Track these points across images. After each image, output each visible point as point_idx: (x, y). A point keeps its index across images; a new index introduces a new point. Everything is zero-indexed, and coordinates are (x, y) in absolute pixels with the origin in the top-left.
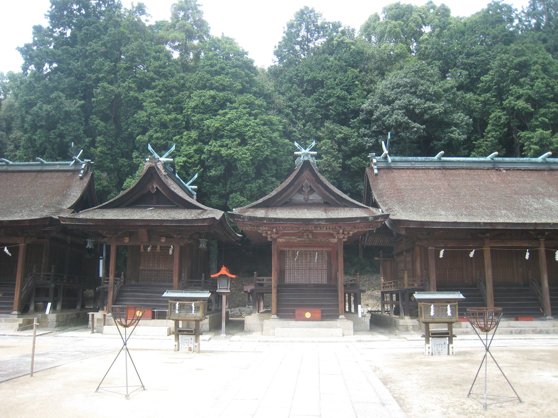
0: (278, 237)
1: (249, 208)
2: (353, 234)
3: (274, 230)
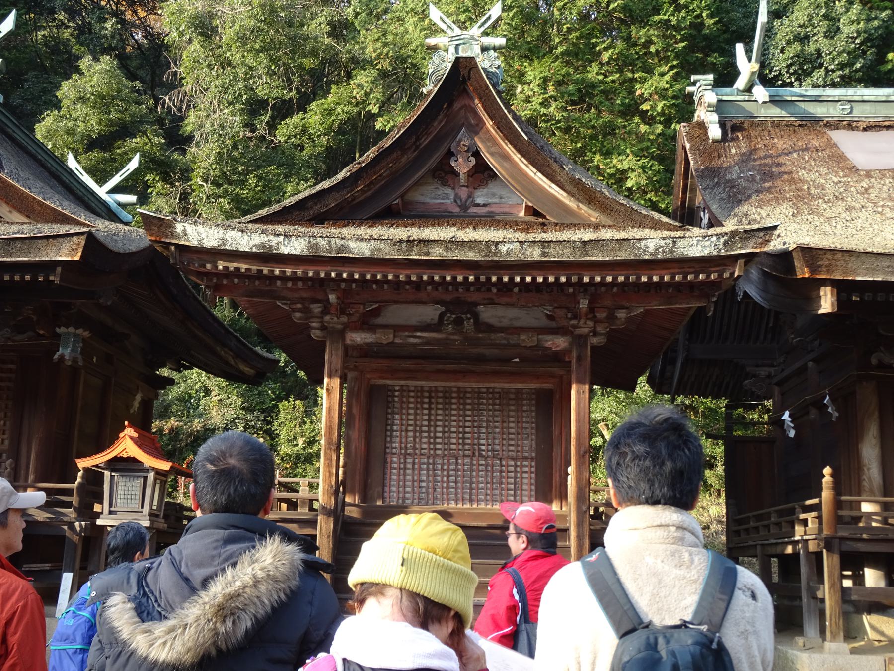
0: (347, 327)
1: (249, 222)
2: (629, 320)
3: (332, 298)
